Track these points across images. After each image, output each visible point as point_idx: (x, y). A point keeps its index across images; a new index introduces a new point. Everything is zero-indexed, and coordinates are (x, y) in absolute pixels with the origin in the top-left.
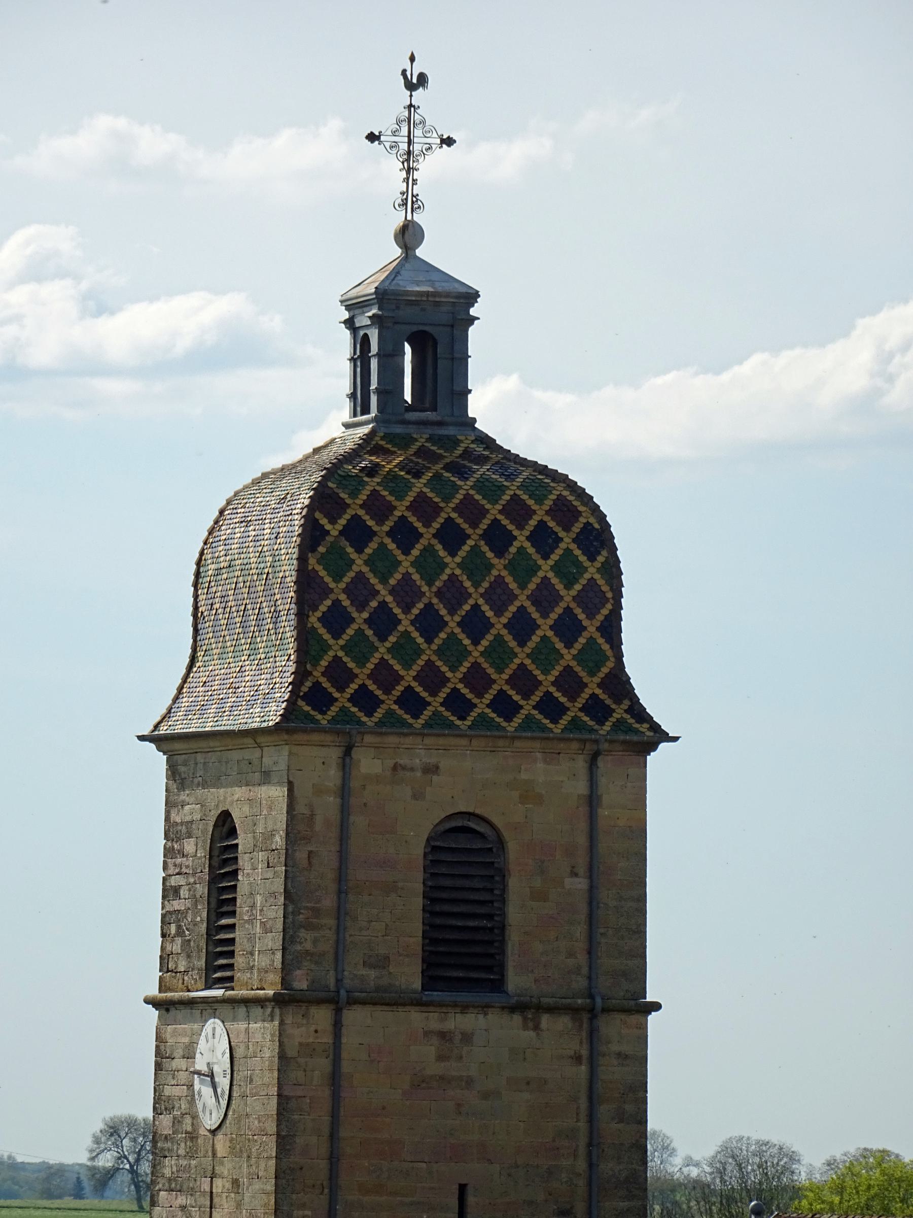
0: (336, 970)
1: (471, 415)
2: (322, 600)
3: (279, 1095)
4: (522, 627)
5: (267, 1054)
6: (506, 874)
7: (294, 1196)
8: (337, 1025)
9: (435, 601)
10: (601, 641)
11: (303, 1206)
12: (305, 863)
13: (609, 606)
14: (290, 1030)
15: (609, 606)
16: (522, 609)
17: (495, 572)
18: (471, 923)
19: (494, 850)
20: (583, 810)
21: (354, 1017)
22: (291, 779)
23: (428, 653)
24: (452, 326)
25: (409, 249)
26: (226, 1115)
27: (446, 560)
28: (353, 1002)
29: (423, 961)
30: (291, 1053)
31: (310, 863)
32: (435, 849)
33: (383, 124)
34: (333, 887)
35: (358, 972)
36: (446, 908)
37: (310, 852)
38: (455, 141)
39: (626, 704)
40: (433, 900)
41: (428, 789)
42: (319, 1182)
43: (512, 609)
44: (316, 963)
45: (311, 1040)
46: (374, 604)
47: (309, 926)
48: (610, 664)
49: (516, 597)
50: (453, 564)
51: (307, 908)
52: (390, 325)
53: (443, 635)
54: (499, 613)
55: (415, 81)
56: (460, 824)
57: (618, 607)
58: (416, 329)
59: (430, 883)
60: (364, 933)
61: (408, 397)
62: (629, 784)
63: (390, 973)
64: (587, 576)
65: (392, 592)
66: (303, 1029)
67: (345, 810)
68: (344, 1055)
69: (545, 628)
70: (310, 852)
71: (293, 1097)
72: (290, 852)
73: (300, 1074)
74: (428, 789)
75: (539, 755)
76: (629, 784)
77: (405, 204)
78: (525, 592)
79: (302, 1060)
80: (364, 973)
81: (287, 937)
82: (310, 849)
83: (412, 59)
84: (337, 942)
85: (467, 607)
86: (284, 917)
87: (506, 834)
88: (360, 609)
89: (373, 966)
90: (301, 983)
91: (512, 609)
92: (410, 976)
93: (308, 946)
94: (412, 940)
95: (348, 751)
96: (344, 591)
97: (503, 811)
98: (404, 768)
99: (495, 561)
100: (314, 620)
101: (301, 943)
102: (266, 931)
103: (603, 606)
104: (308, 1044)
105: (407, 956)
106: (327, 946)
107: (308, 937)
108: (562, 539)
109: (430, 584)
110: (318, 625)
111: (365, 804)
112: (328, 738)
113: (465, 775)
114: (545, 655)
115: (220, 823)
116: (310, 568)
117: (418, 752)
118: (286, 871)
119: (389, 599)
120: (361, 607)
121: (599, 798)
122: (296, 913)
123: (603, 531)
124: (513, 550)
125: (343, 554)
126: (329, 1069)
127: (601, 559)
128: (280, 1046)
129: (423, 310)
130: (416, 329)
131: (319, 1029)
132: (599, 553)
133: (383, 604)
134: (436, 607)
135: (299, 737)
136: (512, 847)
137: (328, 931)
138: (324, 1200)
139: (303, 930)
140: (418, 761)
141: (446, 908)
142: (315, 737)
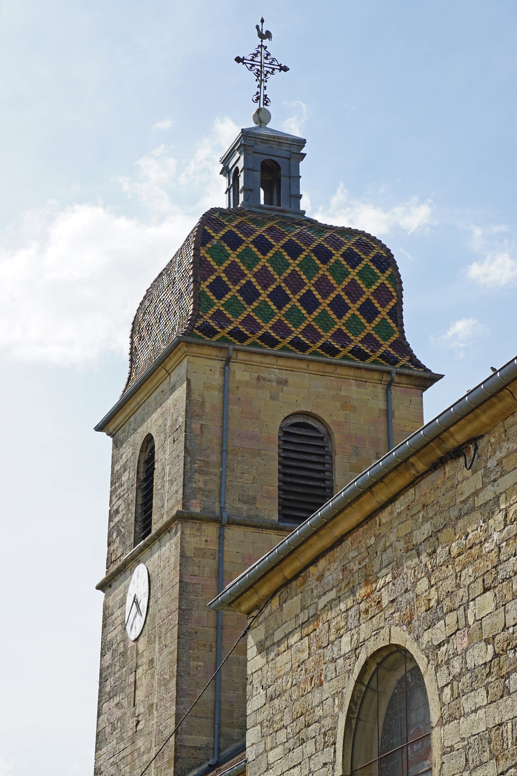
0: (220, 502)
1: (302, 208)
2: (209, 275)
3: (181, 582)
4: (339, 306)
5: (173, 559)
6: (333, 455)
7: (191, 651)
8: (221, 538)
9: (283, 285)
10: (390, 321)
11: (198, 659)
12: (198, 432)
13: (394, 301)
14: (188, 539)
15: (394, 301)
16: (339, 296)
17: (321, 272)
18: (311, 483)
19: (325, 439)
20: (383, 419)
21: (233, 534)
22: (189, 377)
23: (279, 315)
24: (289, 159)
25: (263, 122)
26: (145, 621)
27: (290, 261)
28: (232, 523)
29: (279, 504)
30: (189, 553)
31: (202, 432)
32: (286, 433)
33: (247, 55)
34: (218, 448)
35: (234, 506)
36: (294, 472)
37: (202, 425)
38: (289, 69)
39: (408, 358)
40: (285, 466)
41: (281, 394)
42: (209, 643)
43: (333, 295)
44: (206, 496)
45: (203, 547)
46: (243, 282)
47: (201, 472)
48: (397, 335)
49: (335, 289)
50: (294, 265)
51: (200, 460)
52: (251, 152)
53: (288, 306)
54: (324, 297)
55: (264, 33)
56: (302, 421)
57: (400, 303)
58: (268, 163)
59: (283, 455)
60: (238, 480)
61: (262, 202)
62: (412, 406)
63: (257, 508)
64: (380, 281)
65: (255, 276)
66: (198, 538)
67: (225, 402)
68: (226, 559)
69: (354, 309)
70: (202, 425)
71: (190, 583)
72: (188, 423)
73: (196, 568)
74: (281, 394)
75: (353, 382)
76: (412, 406)
77: (258, 98)
78: (341, 286)
79: (197, 560)
80: (239, 506)
81: (186, 478)
82: (202, 423)
83: (262, 21)
84: (221, 484)
85: (304, 291)
86: (184, 464)
87: (333, 428)
88: (235, 283)
89: (245, 502)
90: (196, 509)
91: (333, 295)
92: (271, 511)
93: (201, 485)
94: (271, 488)
95: (228, 361)
96: (224, 271)
97: (330, 413)
98: (265, 379)
99: (321, 266)
100: (204, 286)
101: (195, 482)
102: (171, 482)
103: (391, 300)
104: (201, 549)
105: (268, 498)
106: (213, 487)
107: (201, 479)
108: (363, 259)
109: (280, 274)
110: (206, 290)
111: (239, 399)
112: (214, 352)
113: (305, 388)
114: (354, 325)
115: (144, 450)
116: (201, 255)
117: (273, 369)
118: (185, 435)
119: (253, 280)
120: (235, 282)
121: (393, 412)
122: (192, 462)
123: (389, 258)
124: (332, 261)
125: (222, 250)
126: (215, 567)
127: (388, 272)
128: (181, 548)
129: (271, 147)
130: (268, 163)
131: (208, 539)
132: (387, 269)
133: (249, 282)
134: (283, 288)
135: (195, 350)
136: (337, 437)
137: (214, 477)
138: (212, 655)
139: (197, 474)
140: (273, 376)
141: (294, 472)
142: (206, 351)
